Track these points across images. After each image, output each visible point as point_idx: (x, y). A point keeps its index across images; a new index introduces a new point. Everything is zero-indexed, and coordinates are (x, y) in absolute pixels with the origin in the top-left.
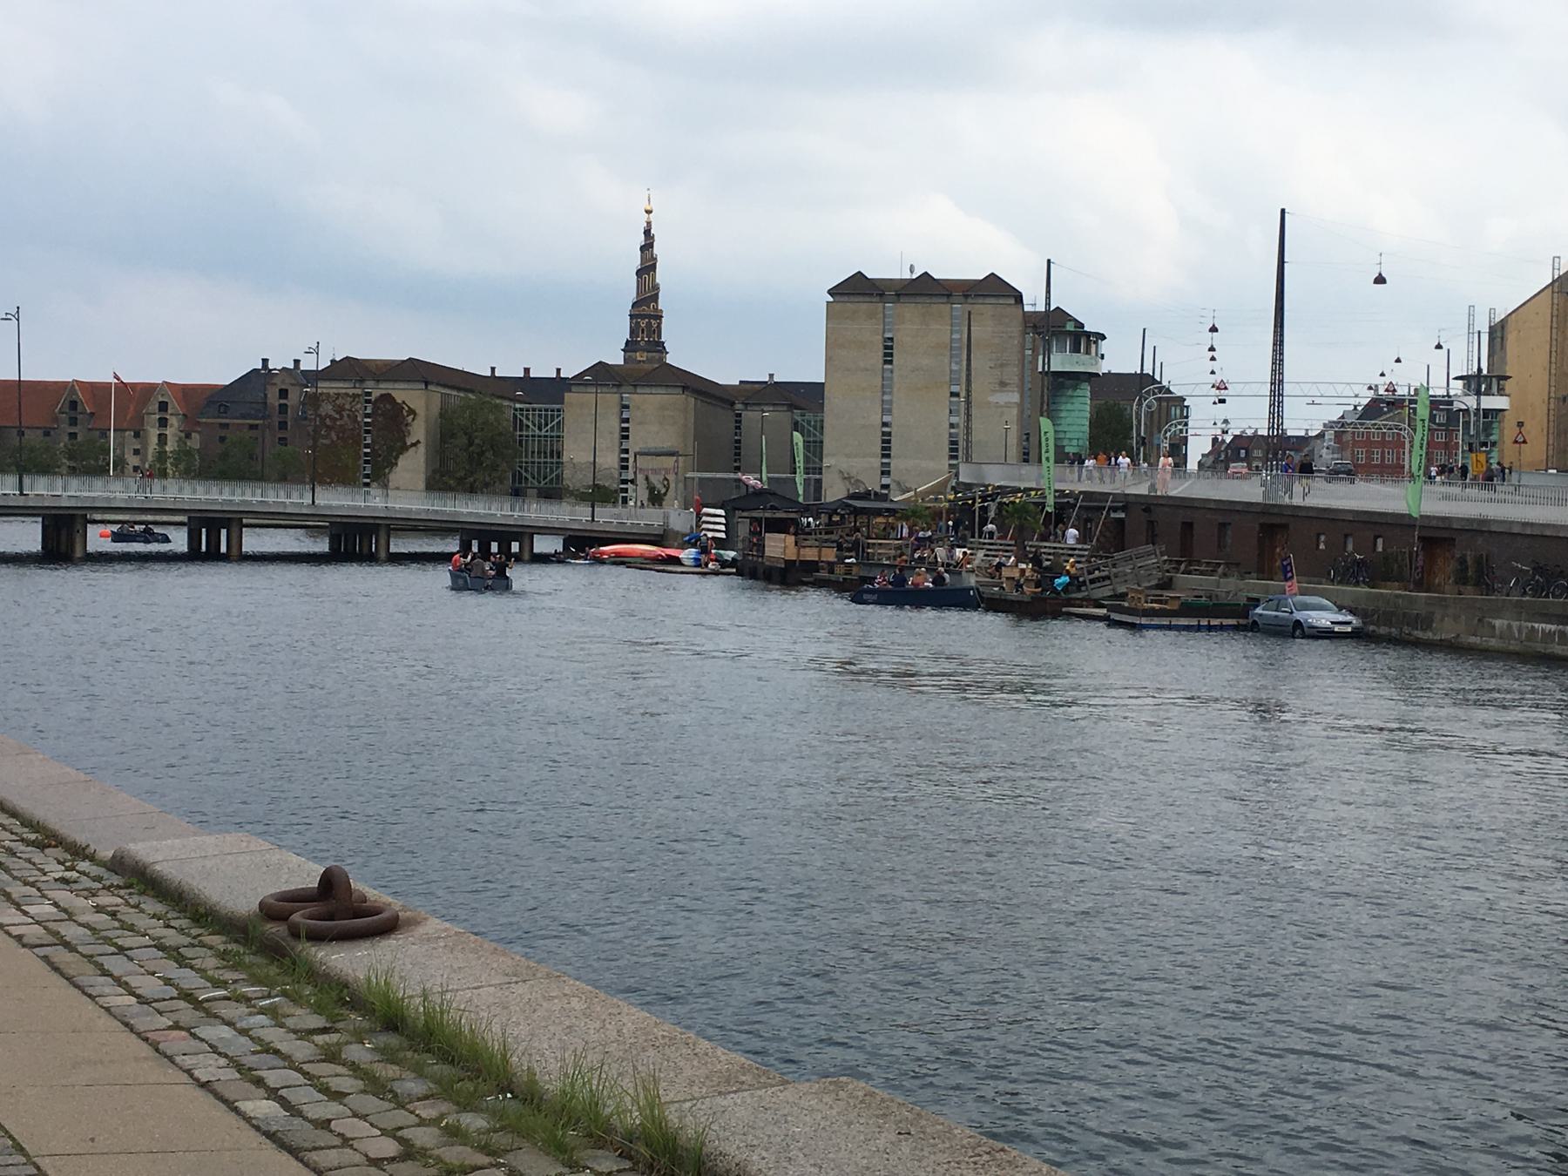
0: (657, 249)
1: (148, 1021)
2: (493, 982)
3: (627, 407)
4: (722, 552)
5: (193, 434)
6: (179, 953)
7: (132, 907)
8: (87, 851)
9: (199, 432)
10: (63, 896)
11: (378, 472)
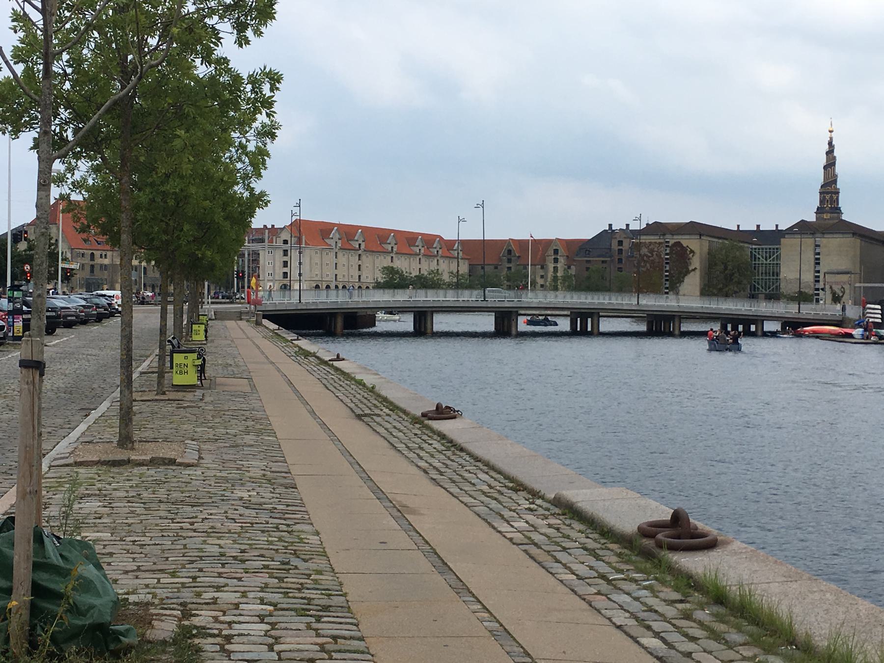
0: (836, 153)
1: (583, 589)
2: (777, 580)
3: (819, 246)
4: (879, 330)
5: (572, 266)
6: (595, 552)
7: (567, 526)
8: (540, 494)
9: (574, 265)
10: (530, 517)
11: (673, 285)
